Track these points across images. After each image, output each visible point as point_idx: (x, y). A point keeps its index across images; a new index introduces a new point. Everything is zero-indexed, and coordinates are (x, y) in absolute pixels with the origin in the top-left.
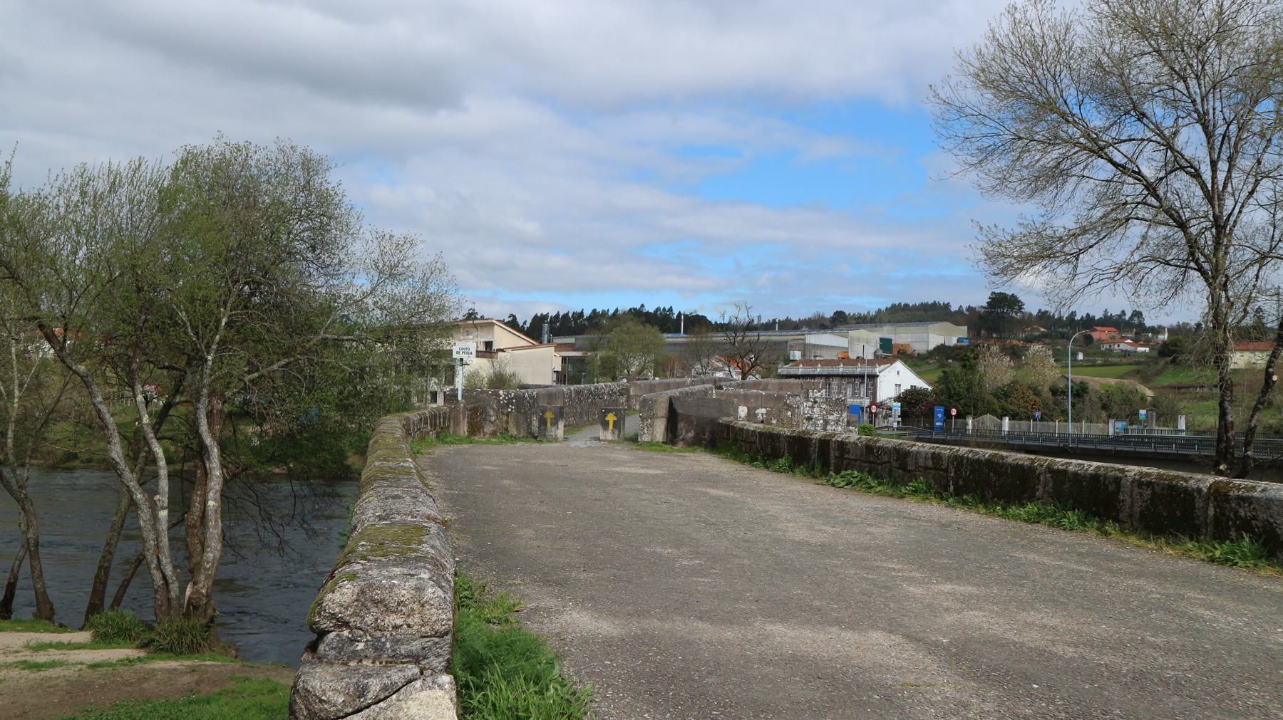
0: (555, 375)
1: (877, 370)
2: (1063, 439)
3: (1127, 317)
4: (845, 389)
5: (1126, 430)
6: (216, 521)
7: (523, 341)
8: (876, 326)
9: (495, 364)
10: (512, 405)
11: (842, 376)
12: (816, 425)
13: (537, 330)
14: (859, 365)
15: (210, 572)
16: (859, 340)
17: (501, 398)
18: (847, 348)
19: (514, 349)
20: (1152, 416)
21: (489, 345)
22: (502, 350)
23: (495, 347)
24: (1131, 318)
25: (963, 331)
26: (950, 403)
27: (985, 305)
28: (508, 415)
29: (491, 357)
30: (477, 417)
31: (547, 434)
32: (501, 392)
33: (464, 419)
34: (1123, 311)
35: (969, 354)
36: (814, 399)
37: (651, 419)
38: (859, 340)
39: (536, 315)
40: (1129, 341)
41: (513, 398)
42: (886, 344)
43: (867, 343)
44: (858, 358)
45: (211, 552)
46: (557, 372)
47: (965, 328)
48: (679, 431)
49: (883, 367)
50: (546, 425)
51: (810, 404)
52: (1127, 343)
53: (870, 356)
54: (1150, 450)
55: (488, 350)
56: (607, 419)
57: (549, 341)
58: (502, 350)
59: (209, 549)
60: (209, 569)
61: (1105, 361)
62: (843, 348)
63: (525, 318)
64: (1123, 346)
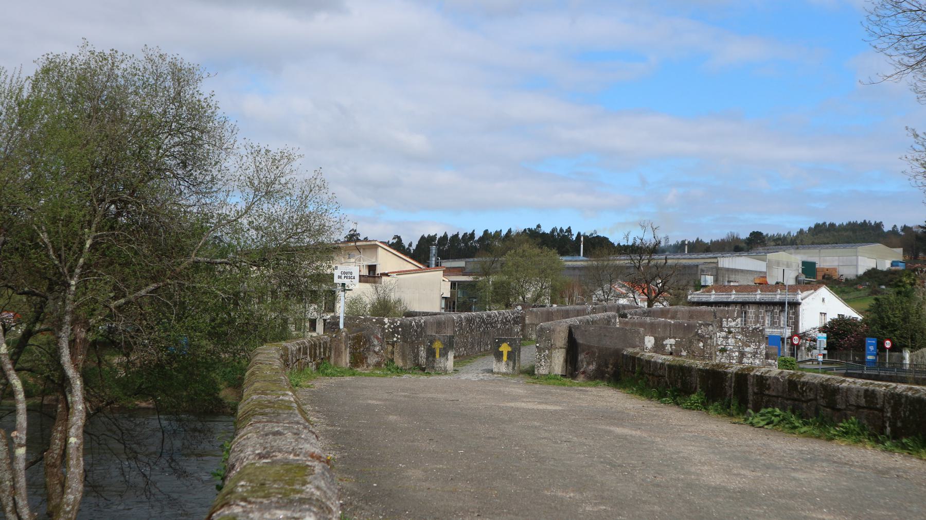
0: (443, 302)
1: (799, 297)
4: (763, 318)
6: (78, 459)
7: (408, 265)
9: (379, 289)
11: (760, 304)
12: (730, 357)
14: (779, 291)
15: (70, 516)
16: (778, 264)
17: (386, 326)
18: (765, 273)
19: (400, 273)
21: (372, 268)
22: (387, 275)
23: (379, 271)
25: (898, 254)
28: (393, 344)
29: (375, 282)
30: (360, 347)
31: (435, 365)
33: (345, 349)
36: (729, 328)
37: (549, 350)
41: (398, 327)
42: (809, 268)
44: (777, 283)
45: (71, 493)
46: (446, 298)
47: (902, 249)
49: (805, 293)
50: (434, 356)
51: (724, 334)
55: (372, 275)
56: (501, 349)
57: (437, 265)
58: (387, 275)
59: (69, 491)
60: (69, 512)
62: (761, 272)
63: (411, 239)
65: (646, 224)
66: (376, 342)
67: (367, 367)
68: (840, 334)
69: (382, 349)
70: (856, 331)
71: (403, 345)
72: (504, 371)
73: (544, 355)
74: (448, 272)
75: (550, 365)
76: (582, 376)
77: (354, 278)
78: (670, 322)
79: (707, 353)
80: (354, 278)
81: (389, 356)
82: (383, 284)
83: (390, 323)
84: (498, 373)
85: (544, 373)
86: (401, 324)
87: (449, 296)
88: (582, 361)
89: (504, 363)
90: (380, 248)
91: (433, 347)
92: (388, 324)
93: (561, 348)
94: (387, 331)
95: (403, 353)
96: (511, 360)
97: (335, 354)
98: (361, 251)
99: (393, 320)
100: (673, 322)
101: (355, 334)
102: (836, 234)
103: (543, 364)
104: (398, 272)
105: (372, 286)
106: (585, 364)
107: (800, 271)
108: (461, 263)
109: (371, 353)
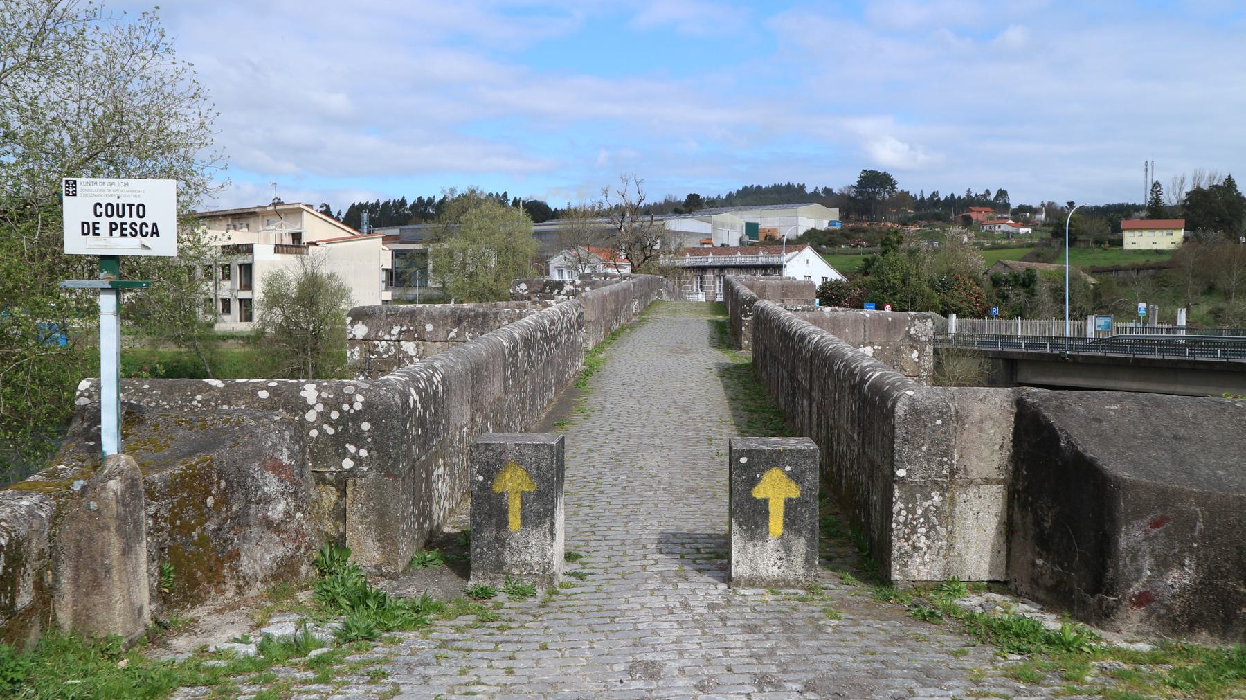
0: (384, 274)
2: (1058, 342)
3: (992, 197)
5: (1109, 326)
7: (342, 232)
8: (740, 209)
9: (306, 261)
10: (359, 445)
13: (356, 218)
14: (761, 253)
16: (723, 225)
17: (311, 416)
18: (711, 235)
19: (330, 241)
20: (1154, 311)
21: (297, 236)
22: (314, 244)
23: (305, 240)
24: (996, 198)
25: (835, 213)
26: (883, 299)
27: (856, 184)
28: (341, 482)
29: (300, 253)
30: (203, 518)
31: (507, 557)
32: (310, 392)
33: (127, 551)
34: (988, 191)
35: (892, 237)
37: (943, 490)
38: (723, 225)
39: (354, 204)
40: (1011, 222)
41: (358, 417)
42: (752, 229)
43: (732, 228)
44: (723, 245)
46: (386, 270)
47: (837, 210)
48: (1125, 563)
49: (790, 255)
50: (503, 524)
52: (1009, 224)
53: (734, 243)
54: (1183, 358)
55: (297, 244)
56: (758, 493)
57: (369, 233)
58: (314, 244)
61: (993, 244)
62: (706, 234)
63: (341, 206)
64: (1004, 228)
65: (627, 177)
66: (272, 485)
67: (240, 590)
68: (833, 299)
69: (298, 508)
70: (848, 295)
71: (378, 485)
72: (774, 572)
73: (926, 510)
74: (387, 240)
75: (950, 548)
76: (1139, 613)
77: (155, 232)
78: (864, 316)
79: (925, 370)
80: (155, 232)
81: (328, 527)
82: (310, 254)
83: (326, 402)
84: (751, 583)
85: (924, 576)
86: (367, 405)
87: (390, 267)
88: (1135, 555)
89: (772, 543)
90: (304, 212)
91: (497, 489)
92: (320, 408)
93: (987, 481)
94: (314, 433)
95: (381, 515)
96: (799, 532)
97: (75, 580)
98: (283, 216)
99: (339, 391)
100: (868, 316)
101: (178, 469)
102: (762, 196)
103: (923, 542)
104: (328, 240)
105: (297, 258)
106: (1147, 564)
107: (744, 233)
108: (395, 231)
109: (254, 531)
